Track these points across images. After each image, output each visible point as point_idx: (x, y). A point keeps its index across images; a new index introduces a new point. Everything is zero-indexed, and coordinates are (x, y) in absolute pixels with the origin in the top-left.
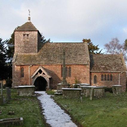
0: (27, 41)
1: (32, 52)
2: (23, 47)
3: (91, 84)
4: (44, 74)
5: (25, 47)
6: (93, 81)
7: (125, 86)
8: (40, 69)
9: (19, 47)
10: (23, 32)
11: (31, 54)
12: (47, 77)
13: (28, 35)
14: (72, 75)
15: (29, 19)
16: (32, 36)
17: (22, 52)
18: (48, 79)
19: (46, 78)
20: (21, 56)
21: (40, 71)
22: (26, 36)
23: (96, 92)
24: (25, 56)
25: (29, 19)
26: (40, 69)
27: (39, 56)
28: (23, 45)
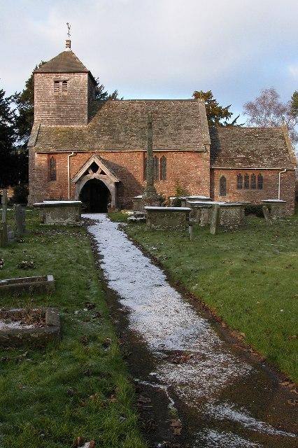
0: (64, 96)
1: (74, 121)
2: (54, 110)
3: (212, 198)
4: (103, 173)
5: (59, 109)
6: (217, 190)
7: (292, 200)
8: (94, 162)
9: (44, 110)
10: (54, 76)
11: (73, 126)
12: (110, 181)
13: (65, 82)
14: (167, 176)
15: (69, 44)
16: (76, 84)
17: (51, 122)
18: (113, 185)
19: (107, 183)
20: (49, 132)
21: (94, 167)
22: (61, 84)
23: (225, 216)
24: (58, 131)
25: (69, 44)
26: (94, 162)
27: (90, 130)
28: (53, 104)
